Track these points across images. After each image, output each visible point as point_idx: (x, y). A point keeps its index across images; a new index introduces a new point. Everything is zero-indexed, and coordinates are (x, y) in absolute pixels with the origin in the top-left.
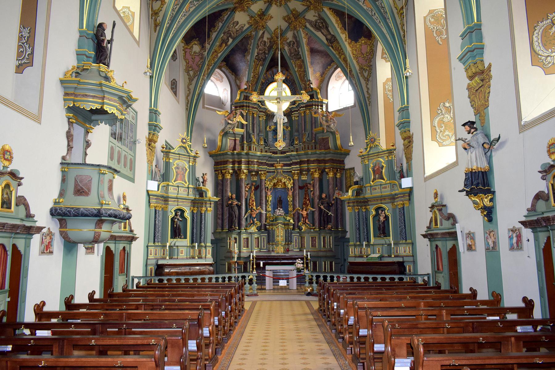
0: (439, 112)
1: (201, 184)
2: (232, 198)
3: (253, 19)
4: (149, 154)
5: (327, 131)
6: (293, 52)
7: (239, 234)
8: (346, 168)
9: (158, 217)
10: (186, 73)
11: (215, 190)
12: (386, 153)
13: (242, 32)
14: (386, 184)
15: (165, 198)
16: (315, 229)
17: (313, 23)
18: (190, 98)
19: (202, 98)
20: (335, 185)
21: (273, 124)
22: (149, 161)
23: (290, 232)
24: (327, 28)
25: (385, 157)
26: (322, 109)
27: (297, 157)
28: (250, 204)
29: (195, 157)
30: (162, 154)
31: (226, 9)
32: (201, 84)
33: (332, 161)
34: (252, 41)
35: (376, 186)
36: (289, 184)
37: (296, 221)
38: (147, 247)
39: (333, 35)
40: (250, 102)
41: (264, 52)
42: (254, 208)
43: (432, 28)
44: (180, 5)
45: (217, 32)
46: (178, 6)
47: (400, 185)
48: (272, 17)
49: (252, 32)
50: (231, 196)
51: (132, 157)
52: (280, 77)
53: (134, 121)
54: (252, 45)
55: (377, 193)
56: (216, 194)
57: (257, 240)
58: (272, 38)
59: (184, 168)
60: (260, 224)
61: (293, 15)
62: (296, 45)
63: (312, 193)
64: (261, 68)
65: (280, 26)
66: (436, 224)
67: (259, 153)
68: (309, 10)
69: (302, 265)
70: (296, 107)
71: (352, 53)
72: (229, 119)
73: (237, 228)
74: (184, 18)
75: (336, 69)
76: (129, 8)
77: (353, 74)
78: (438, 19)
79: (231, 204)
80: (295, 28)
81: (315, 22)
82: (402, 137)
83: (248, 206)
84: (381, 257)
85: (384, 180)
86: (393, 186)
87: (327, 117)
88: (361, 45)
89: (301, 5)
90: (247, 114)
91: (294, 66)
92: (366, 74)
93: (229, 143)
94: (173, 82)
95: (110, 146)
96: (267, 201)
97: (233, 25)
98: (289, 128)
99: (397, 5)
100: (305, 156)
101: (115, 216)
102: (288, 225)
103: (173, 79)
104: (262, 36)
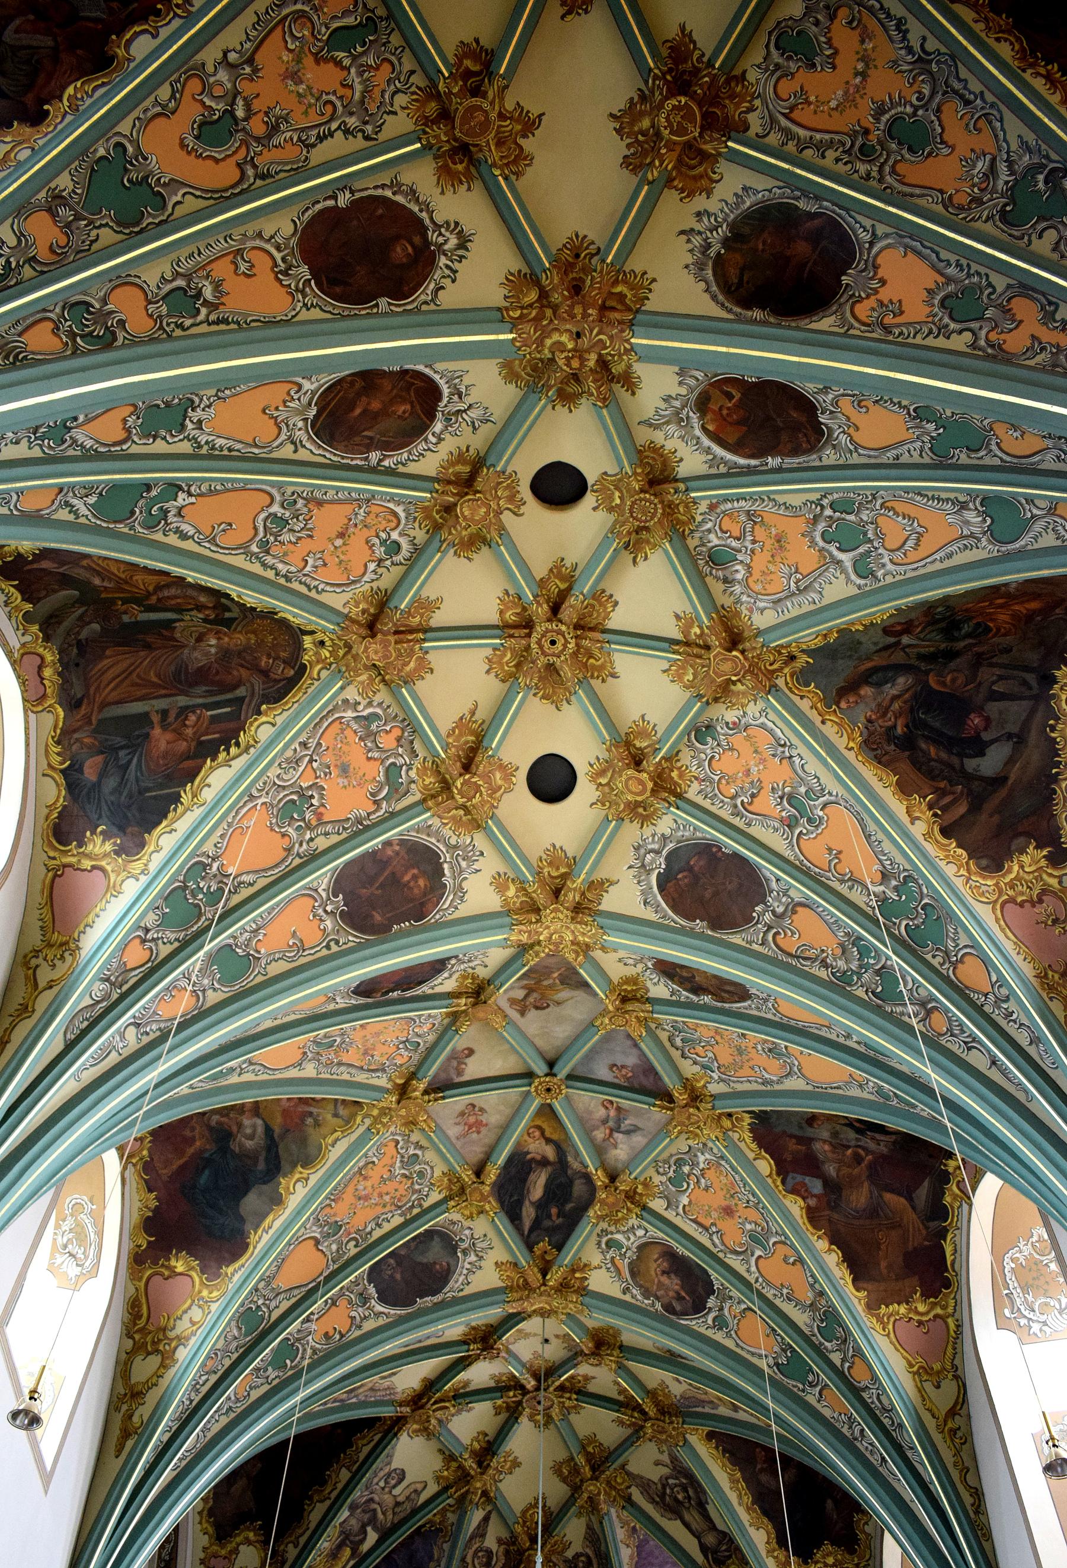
3: (454, 1464)
24: (701, 1506)
34: (446, 1546)
39: (724, 1534)
44: (219, 1373)
45: (328, 1503)
46: (214, 1378)
48: (516, 1464)
49: (449, 1515)
58: (513, 1539)
61: (589, 1457)
68: (638, 1438)
74: (224, 1420)
80: (593, 1503)
81: (659, 1486)
97: (386, 1482)
99: (931, 1401)
104: (481, 1532)
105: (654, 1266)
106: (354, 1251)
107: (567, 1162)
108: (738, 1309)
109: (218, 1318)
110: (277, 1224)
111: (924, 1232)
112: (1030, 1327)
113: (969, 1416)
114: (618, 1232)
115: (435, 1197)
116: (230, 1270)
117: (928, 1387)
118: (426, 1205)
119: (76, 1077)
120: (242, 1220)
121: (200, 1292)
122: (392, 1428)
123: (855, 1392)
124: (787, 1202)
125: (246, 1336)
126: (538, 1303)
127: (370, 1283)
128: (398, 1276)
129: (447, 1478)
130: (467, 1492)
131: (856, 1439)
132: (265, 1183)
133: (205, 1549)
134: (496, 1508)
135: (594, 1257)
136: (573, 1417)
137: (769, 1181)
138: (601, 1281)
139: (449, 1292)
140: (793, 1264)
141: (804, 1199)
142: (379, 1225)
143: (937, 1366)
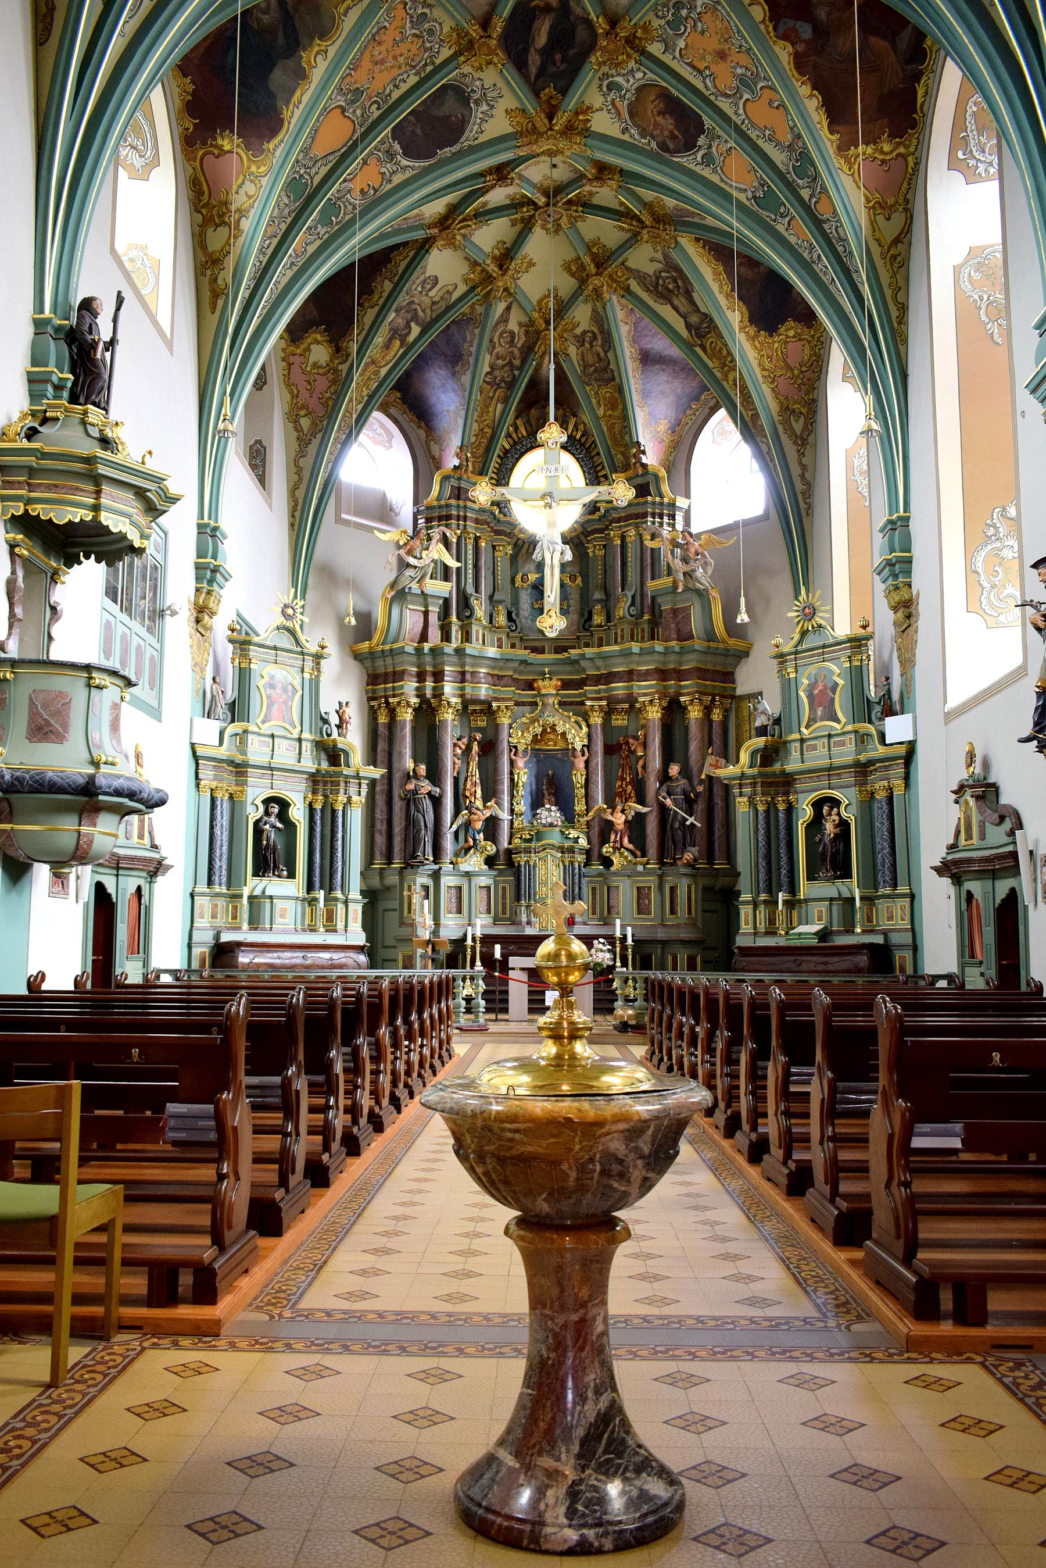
0: (989, 534)
1: (335, 731)
2: (416, 776)
3: (479, 269)
4: (195, 646)
5: (687, 589)
6: (591, 362)
7: (436, 876)
8: (739, 692)
9: (219, 818)
10: (292, 425)
11: (368, 753)
12: (845, 649)
13: (449, 308)
14: (844, 734)
15: (237, 765)
16: (647, 863)
17: (649, 279)
18: (300, 494)
19: (333, 495)
20: (706, 743)
21: (532, 567)
22: (196, 664)
23: (577, 871)
24: (688, 294)
25: (843, 659)
26: (673, 526)
27: (599, 662)
28: (468, 794)
29: (318, 657)
30: (230, 647)
31: (405, 244)
32: (331, 453)
33: (702, 673)
34: (477, 331)
35: (816, 738)
36: (577, 739)
37: (596, 840)
38: (192, 896)
39: (706, 315)
40: (469, 504)
41: (510, 363)
42: (479, 803)
43: (977, 297)
44: (279, 237)
45: (377, 308)
46: (275, 241)
47: (882, 736)
48: (531, 264)
50: (414, 770)
51: (155, 653)
52: (553, 434)
53: (159, 557)
54: (476, 342)
55: (817, 757)
56: (372, 760)
57: (484, 892)
58: (532, 322)
59: (290, 687)
60: (494, 847)
61: (594, 257)
62: (599, 342)
63: (641, 763)
64: (500, 406)
65: (556, 290)
66: (969, 837)
67: (492, 652)
69: (608, 955)
70: (600, 519)
71: (760, 365)
72: (410, 553)
73: (431, 859)
74: (290, 274)
75: (713, 410)
76: (144, 248)
77: (762, 426)
78: (993, 273)
79: (415, 792)
80: (597, 293)
81: (654, 279)
82: (889, 603)
83: (461, 798)
84: (824, 935)
85: (838, 721)
86: (862, 738)
87: (684, 547)
88: (786, 343)
89: (616, 230)
90: (459, 538)
91: (594, 401)
92: (798, 426)
93: (411, 620)
94: (255, 448)
95: (104, 621)
96: (513, 784)
97: (423, 287)
98: (579, 580)
100: (621, 660)
101: (131, 795)
102: (571, 850)
103: (257, 442)
104: (504, 319)
105: (651, 107)
106: (377, 114)
107: (569, 8)
108: (724, 148)
109: (270, 192)
110: (305, 99)
111: (901, 75)
112: (977, 167)
113: (910, 244)
114: (619, 75)
115: (446, 53)
116: (271, 146)
117: (880, 219)
118: (438, 61)
119: (122, 34)
120: (273, 96)
121: (249, 168)
122: (424, 246)
123: (817, 223)
124: (776, 49)
125: (295, 202)
126: (545, 146)
127: (394, 139)
128: (418, 131)
129: (474, 280)
130: (491, 290)
131: (813, 262)
132: (286, 58)
133: (284, 350)
134: (516, 299)
135: (596, 99)
136: (580, 225)
137: (762, 27)
138: (603, 123)
139: (465, 142)
140: (777, 108)
141: (793, 44)
142: (397, 87)
143: (891, 201)
